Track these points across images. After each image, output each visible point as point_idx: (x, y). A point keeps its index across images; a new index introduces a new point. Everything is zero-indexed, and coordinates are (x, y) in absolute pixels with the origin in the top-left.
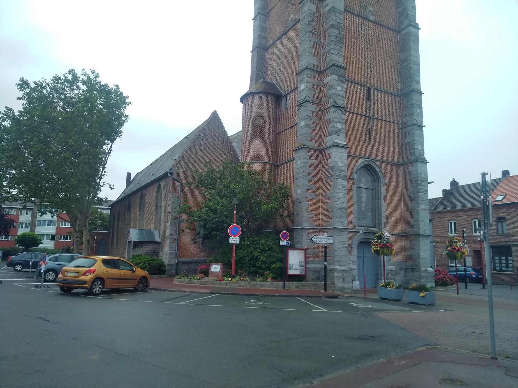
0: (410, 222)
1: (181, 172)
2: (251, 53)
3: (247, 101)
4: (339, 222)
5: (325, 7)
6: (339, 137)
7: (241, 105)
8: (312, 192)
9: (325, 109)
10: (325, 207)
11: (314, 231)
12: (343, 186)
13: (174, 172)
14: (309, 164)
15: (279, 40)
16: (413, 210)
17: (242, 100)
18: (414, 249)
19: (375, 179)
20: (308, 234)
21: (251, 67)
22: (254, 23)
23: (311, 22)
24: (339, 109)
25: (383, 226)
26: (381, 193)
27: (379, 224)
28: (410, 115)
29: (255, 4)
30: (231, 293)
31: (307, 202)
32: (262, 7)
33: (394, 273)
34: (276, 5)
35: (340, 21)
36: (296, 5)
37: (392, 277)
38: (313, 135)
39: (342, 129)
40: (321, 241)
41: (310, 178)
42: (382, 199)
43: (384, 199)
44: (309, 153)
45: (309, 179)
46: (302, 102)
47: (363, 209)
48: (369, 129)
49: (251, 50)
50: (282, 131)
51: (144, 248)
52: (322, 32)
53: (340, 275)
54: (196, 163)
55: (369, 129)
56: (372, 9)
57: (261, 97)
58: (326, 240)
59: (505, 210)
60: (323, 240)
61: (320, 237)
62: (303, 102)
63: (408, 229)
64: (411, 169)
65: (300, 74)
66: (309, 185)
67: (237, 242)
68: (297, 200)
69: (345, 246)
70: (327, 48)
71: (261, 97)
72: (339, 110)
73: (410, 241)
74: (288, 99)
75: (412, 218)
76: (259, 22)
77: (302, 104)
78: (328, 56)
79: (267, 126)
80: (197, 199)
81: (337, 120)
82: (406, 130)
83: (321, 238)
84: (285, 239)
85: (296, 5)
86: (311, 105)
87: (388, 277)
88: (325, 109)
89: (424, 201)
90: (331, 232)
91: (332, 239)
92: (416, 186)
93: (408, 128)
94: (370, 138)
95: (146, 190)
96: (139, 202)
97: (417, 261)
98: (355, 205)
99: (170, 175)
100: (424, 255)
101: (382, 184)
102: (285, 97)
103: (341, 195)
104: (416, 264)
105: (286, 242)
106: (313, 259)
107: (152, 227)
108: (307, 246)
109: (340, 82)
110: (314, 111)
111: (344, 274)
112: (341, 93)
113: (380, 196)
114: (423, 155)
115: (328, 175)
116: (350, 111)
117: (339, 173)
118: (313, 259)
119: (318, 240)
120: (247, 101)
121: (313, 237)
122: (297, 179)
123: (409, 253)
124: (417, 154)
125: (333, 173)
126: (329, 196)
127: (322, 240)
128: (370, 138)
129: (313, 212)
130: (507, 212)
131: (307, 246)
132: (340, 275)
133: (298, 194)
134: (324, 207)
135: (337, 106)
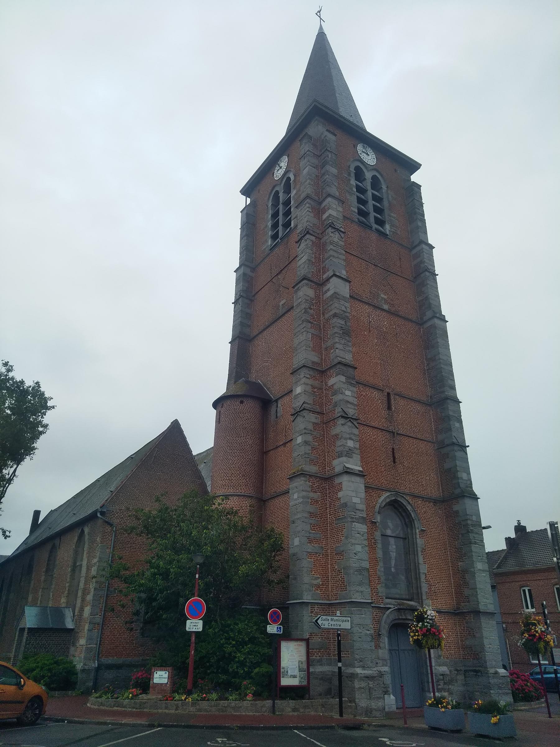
3: (222, 407)
5: (326, 292)
6: (351, 460)
10: (336, 567)
12: (362, 533)
14: (311, 499)
20: (311, 612)
22: (234, 308)
23: (308, 310)
24: (350, 420)
25: (424, 597)
31: (308, 559)
33: (449, 680)
35: (345, 310)
36: (289, 289)
37: (446, 687)
38: (315, 457)
39: (355, 448)
40: (331, 625)
43: (422, 555)
45: (311, 521)
47: (393, 570)
48: (393, 449)
50: (272, 448)
53: (363, 684)
58: (339, 623)
60: (335, 623)
61: (329, 618)
62: (301, 409)
64: (456, 508)
67: (198, 629)
69: (368, 632)
71: (242, 402)
72: (350, 422)
73: (467, 623)
74: (279, 405)
81: (348, 436)
83: (332, 620)
84: (275, 622)
85: (289, 289)
86: (311, 414)
87: (440, 687)
89: (479, 558)
90: (347, 608)
91: (349, 620)
94: (394, 462)
99: (101, 515)
100: (490, 646)
102: (275, 402)
103: (358, 548)
105: (277, 627)
106: (319, 656)
109: (349, 385)
110: (315, 423)
111: (370, 683)
112: (351, 399)
114: (472, 488)
116: (365, 423)
117: (354, 514)
118: (319, 656)
119: (326, 623)
124: (462, 485)
126: (342, 549)
127: (333, 623)
129: (318, 576)
132: (363, 684)
133: (296, 546)
135: (347, 416)
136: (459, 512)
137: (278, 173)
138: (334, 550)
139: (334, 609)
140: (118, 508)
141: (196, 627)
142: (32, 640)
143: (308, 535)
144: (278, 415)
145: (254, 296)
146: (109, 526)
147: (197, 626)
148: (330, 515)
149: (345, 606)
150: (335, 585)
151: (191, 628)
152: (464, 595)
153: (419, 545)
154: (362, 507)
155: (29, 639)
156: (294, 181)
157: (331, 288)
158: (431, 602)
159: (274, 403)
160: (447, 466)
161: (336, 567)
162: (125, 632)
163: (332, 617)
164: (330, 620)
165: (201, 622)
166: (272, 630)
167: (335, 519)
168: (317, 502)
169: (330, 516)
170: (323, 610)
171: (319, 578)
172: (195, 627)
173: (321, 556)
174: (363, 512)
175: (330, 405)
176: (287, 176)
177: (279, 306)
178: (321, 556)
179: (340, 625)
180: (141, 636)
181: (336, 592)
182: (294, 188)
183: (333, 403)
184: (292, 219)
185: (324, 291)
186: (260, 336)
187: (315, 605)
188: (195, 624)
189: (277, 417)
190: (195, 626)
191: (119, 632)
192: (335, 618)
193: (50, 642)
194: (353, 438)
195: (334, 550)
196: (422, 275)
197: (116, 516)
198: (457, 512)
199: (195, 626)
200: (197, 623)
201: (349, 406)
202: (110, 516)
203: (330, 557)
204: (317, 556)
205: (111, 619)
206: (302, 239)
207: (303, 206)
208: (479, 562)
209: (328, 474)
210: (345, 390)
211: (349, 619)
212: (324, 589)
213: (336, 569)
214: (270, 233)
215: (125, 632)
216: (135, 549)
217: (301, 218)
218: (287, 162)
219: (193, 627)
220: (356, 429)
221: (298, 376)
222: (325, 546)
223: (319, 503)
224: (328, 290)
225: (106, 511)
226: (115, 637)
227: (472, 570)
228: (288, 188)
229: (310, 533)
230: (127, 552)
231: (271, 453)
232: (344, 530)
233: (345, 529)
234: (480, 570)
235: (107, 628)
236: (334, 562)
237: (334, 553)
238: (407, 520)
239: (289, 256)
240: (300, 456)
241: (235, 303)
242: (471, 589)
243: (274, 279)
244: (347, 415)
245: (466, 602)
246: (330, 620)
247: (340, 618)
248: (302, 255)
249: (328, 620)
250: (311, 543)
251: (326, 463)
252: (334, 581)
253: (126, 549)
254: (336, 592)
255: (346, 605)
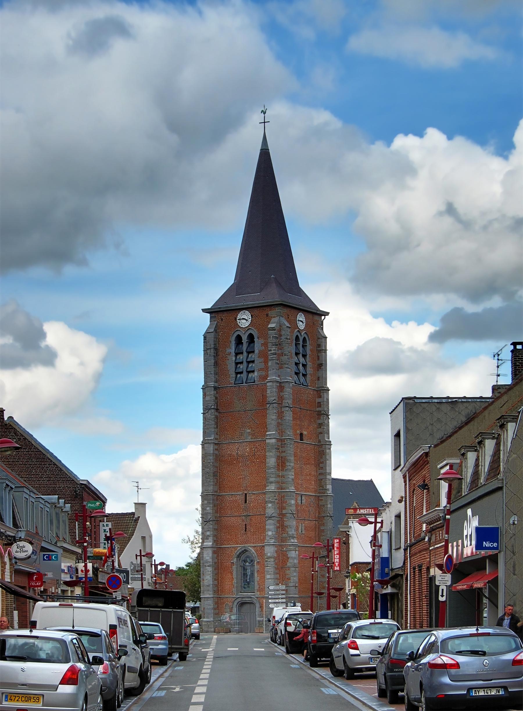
47: (248, 580)
48: (246, 524)
53: (205, 623)
55: (246, 524)
56: (249, 431)
81: (207, 530)
94: (246, 531)
98: (235, 580)
101: (256, 562)
112: (209, 512)
116: (231, 515)
128: (246, 531)
132: (205, 623)
154: (211, 560)
200: (445, 576)
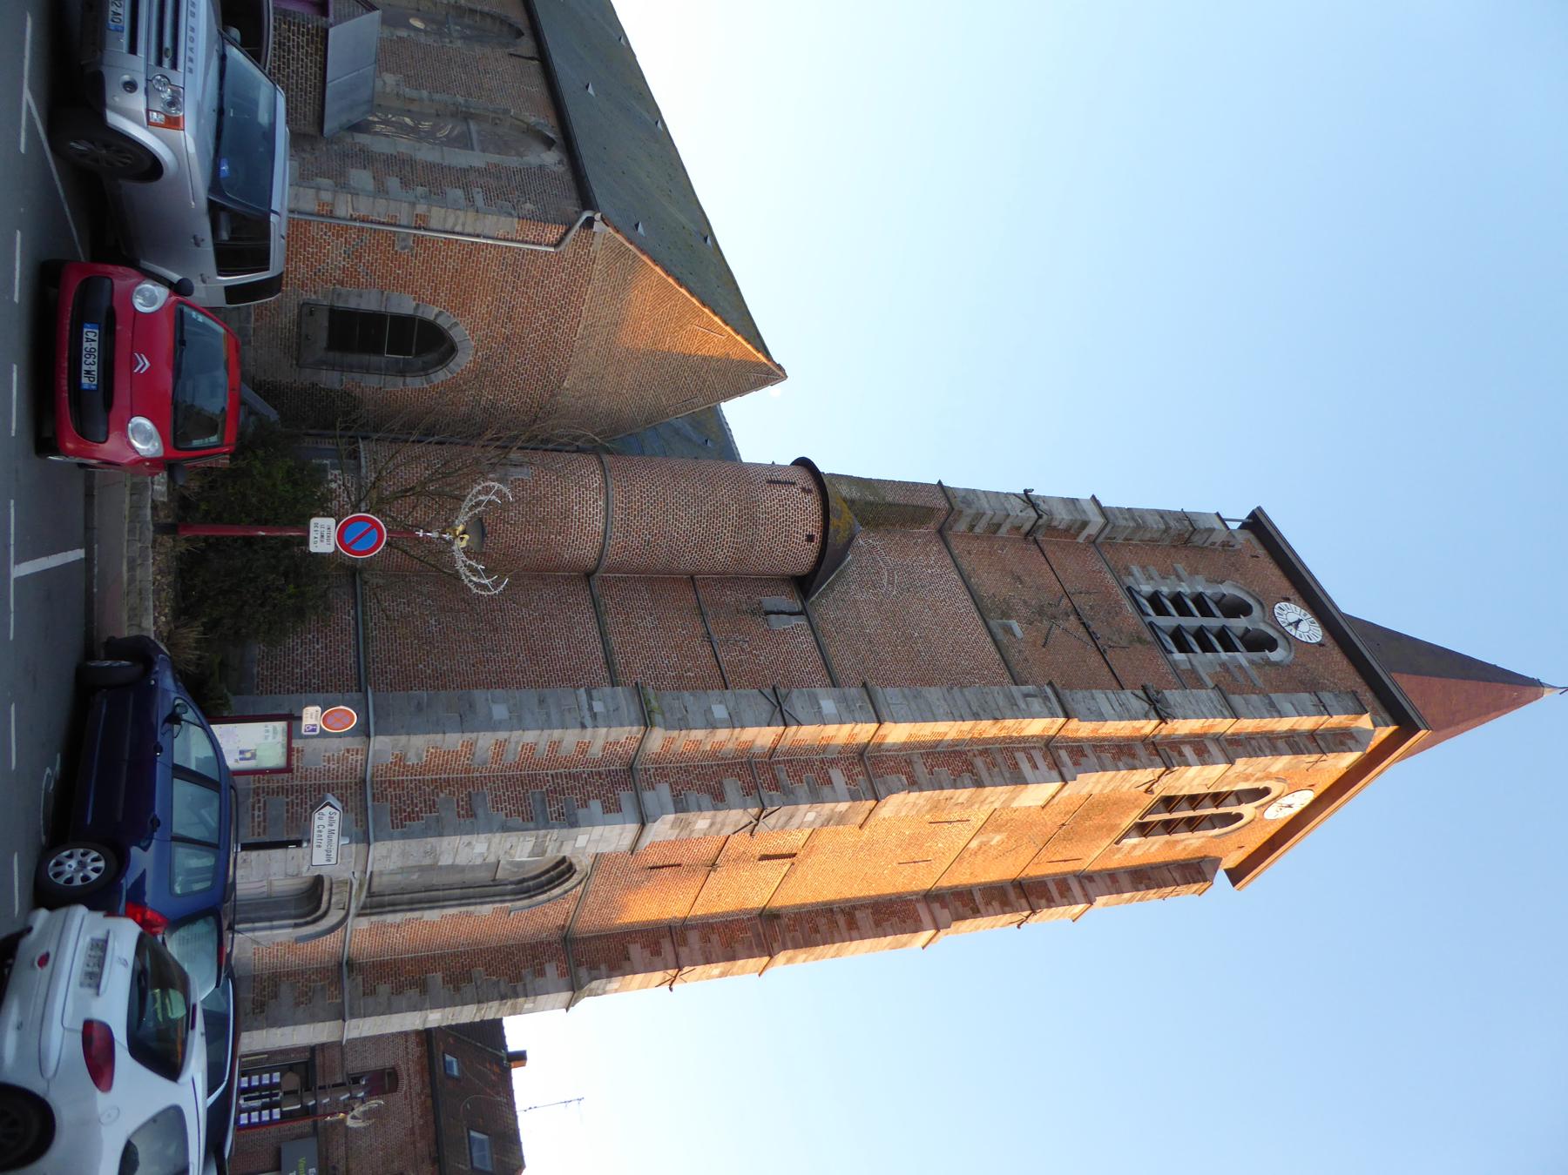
0: (385, 983)
1: (592, 255)
2: (936, 483)
3: (804, 490)
4: (398, 466)
5: (1031, 759)
7: (786, 460)
8: (494, 753)
9: (754, 778)
10: (442, 795)
11: (356, 766)
12: (512, 851)
13: (594, 233)
14: (590, 742)
15: (960, 583)
16: (423, 987)
17: (804, 463)
18: (297, 1004)
19: (525, 884)
21: (897, 480)
22: (1014, 494)
25: (374, 918)
26: (482, 903)
27: (382, 905)
28: (705, 952)
29: (1063, 498)
30: (92, 593)
32: (1055, 523)
34: (1052, 569)
35: (987, 801)
36: (1044, 646)
39: (692, 832)
40: (320, 831)
41: (543, 747)
42: (463, 909)
44: (627, 738)
46: (784, 708)
49: (945, 484)
50: (701, 597)
51: (298, 68)
52: (969, 751)
54: (619, 306)
57: (810, 538)
59: (418, 1088)
61: (336, 827)
62: (784, 712)
63: (363, 979)
64: (551, 970)
65: (866, 697)
66: (521, 744)
67: (315, 543)
68: (470, 706)
70: (923, 772)
71: (810, 538)
73: (323, 988)
74: (794, 621)
75: (398, 990)
76: (1017, 516)
77: (778, 708)
78: (904, 777)
79: (720, 556)
80: (489, 298)
82: (667, 946)
83: (332, 832)
85: (1044, 646)
86: (774, 737)
88: (754, 778)
90: (355, 828)
91: (329, 861)
92: (499, 992)
93: (672, 948)
95: (532, 59)
96: (486, 9)
97: (256, 1020)
102: (800, 606)
104: (246, 1015)
105: (315, 725)
107: (385, 83)
108: (302, 751)
113: (473, 901)
114: (588, 996)
115: (549, 801)
119: (325, 821)
120: (804, 490)
121: (334, 808)
122: (542, 701)
123: (285, 989)
124: (595, 984)
125: (554, 821)
126: (480, 812)
127: (325, 834)
130: (410, 1095)
131: (302, 751)
133: (490, 709)
134: (442, 792)
135: (762, 817)
136: (542, 976)
137: (1290, 613)
138: (478, 789)
139: (353, 791)
140: (598, 256)
141: (318, 540)
142: (298, 38)
143: (512, 740)
144: (773, 617)
145: (1036, 541)
146: (558, 236)
147: (322, 541)
148: (552, 775)
149: (359, 824)
150: (405, 792)
151: (316, 529)
152: (378, 983)
153: (479, 907)
155: (302, 29)
156: (1269, 663)
157: (1037, 772)
158: (365, 928)
159: (799, 603)
160: (635, 951)
161: (442, 795)
162: (311, 270)
163: (336, 832)
164: (330, 828)
165: (329, 549)
166: (309, 715)
167: (544, 790)
168: (584, 752)
169: (550, 778)
170: (351, 769)
171: (421, 759)
172: (319, 536)
173: (466, 762)
174: (555, 851)
175: (789, 777)
176: (1281, 642)
177: (1010, 617)
178: (466, 762)
179: (319, 846)
180: (301, 302)
181: (389, 797)
182: (1252, 662)
183: (792, 784)
184: (1190, 655)
185: (1033, 752)
186: (948, 560)
187: (362, 755)
188: (325, 535)
189: (768, 613)
190: (322, 536)
191: (312, 257)
192: (335, 837)
193: (292, 79)
194: (714, 829)
195: (478, 789)
196: (1023, 902)
197: (580, 250)
198: (541, 973)
199: (322, 536)
200: (328, 540)
201: (783, 819)
202: (581, 239)
203: (465, 778)
204: (468, 756)
205: (343, 240)
206: (1150, 705)
207: (1219, 707)
208: (442, 1016)
209: (641, 769)
210: (817, 812)
211: (333, 861)
212: (397, 768)
213: (438, 796)
214: (1165, 590)
215: (311, 270)
216: (501, 291)
217: (1193, 701)
218: (1309, 641)
219: (319, 533)
220: (733, 832)
221: (858, 705)
222: (487, 768)
223: (580, 756)
224: (1035, 767)
225: (594, 230)
226: (300, 247)
227: (427, 1005)
228: (1259, 643)
229: (517, 743)
230: (495, 274)
231: (692, 595)
232: (520, 819)
233: (523, 820)
234: (427, 1017)
235: (322, 231)
236: (452, 789)
237: (471, 790)
238: (531, 883)
239: (1113, 647)
240: (685, 713)
241: (1028, 498)
242: (389, 999)
243: (1067, 600)
244: (764, 818)
245: (364, 986)
246: (330, 828)
247: (335, 847)
248: (1116, 705)
249: (331, 825)
250: (496, 744)
251: (665, 765)
252: (412, 789)
253: (502, 271)
254: (389, 797)
255: (362, 826)
